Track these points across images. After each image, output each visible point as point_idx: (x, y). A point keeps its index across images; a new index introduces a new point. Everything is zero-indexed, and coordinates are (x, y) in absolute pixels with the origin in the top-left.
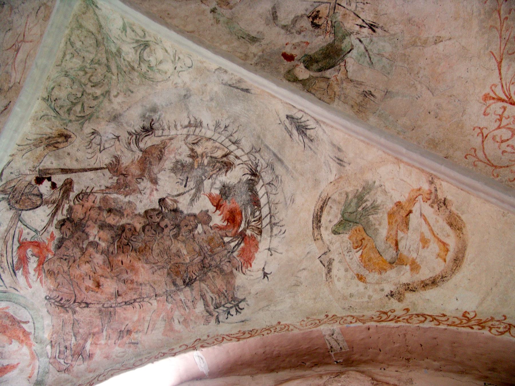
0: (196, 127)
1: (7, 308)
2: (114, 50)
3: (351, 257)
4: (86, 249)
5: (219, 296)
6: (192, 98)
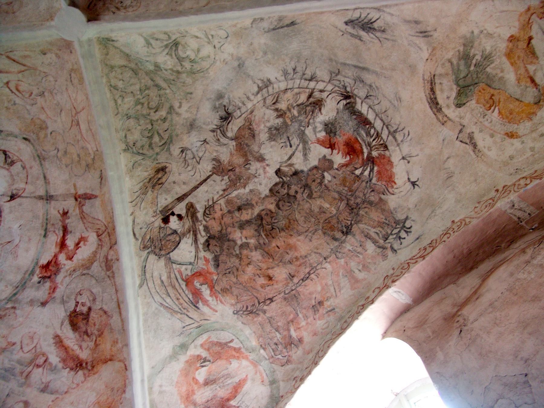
0: (267, 87)
1: (209, 338)
2: (152, 68)
3: (489, 120)
4: (241, 253)
5: (382, 228)
6: (247, 63)
